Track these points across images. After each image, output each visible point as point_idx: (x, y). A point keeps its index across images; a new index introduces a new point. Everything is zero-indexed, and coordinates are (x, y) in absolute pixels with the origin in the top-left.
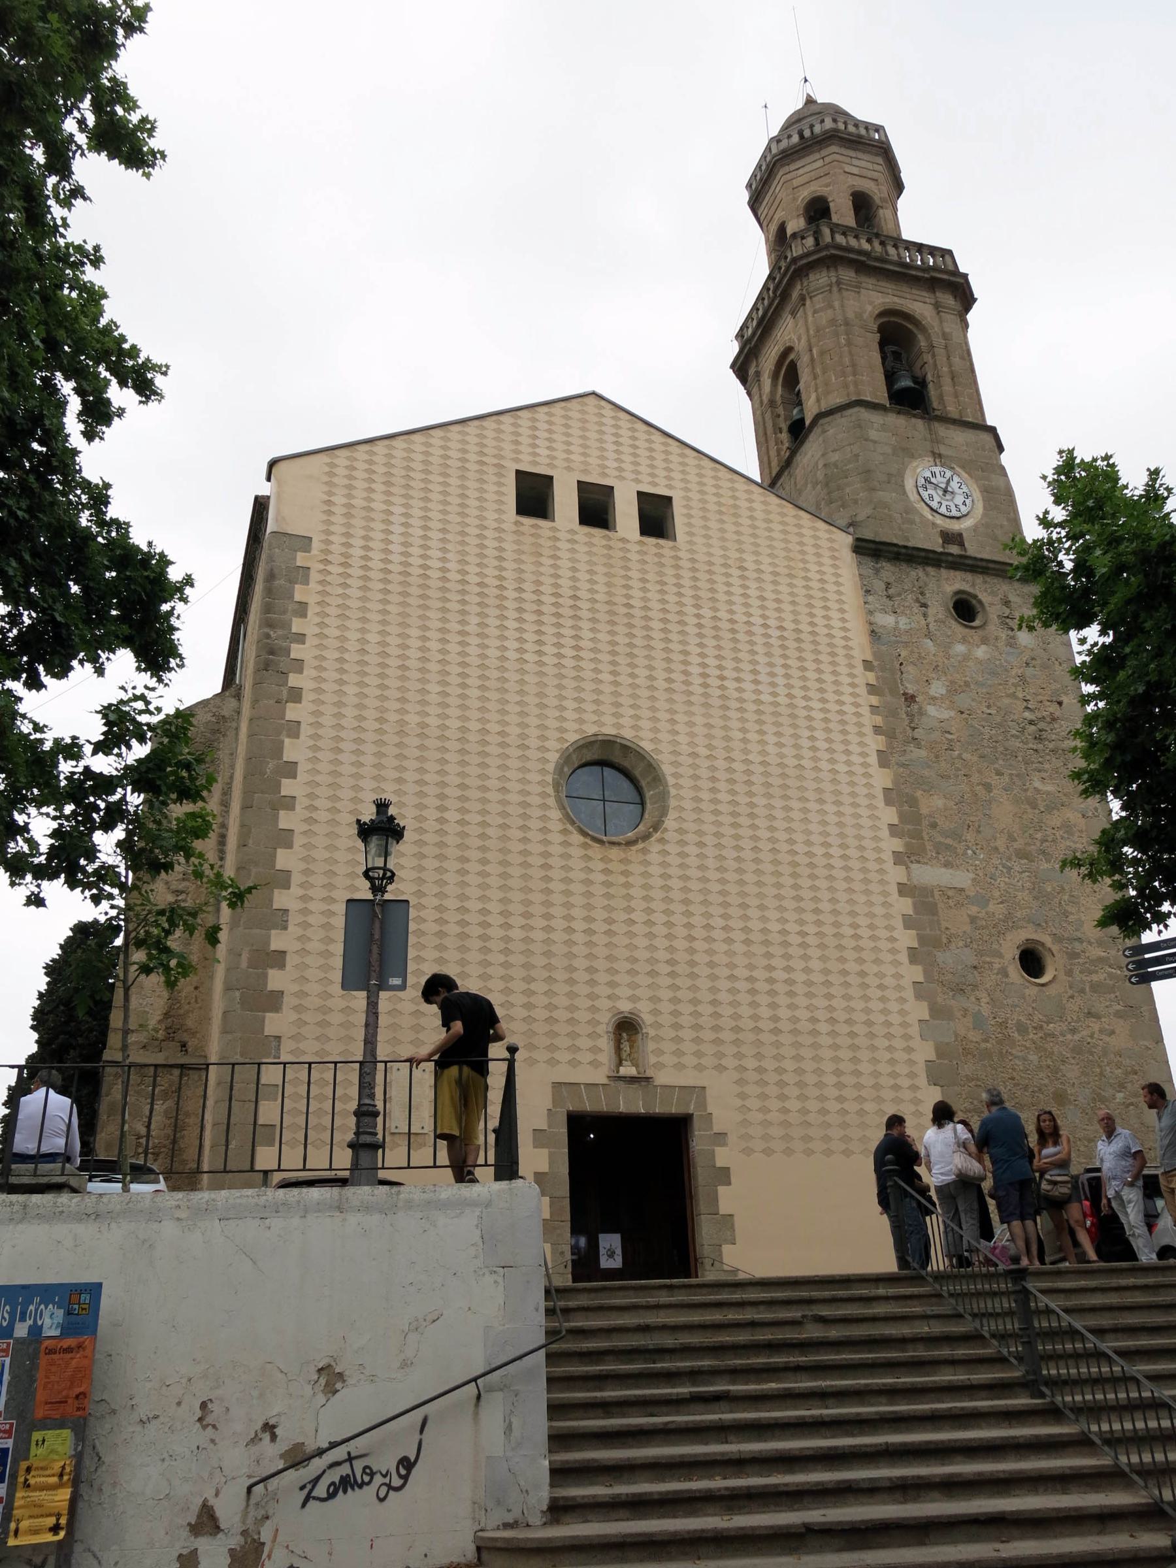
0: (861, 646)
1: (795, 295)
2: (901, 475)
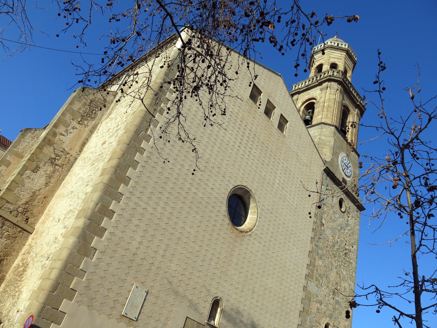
1: (325, 85)
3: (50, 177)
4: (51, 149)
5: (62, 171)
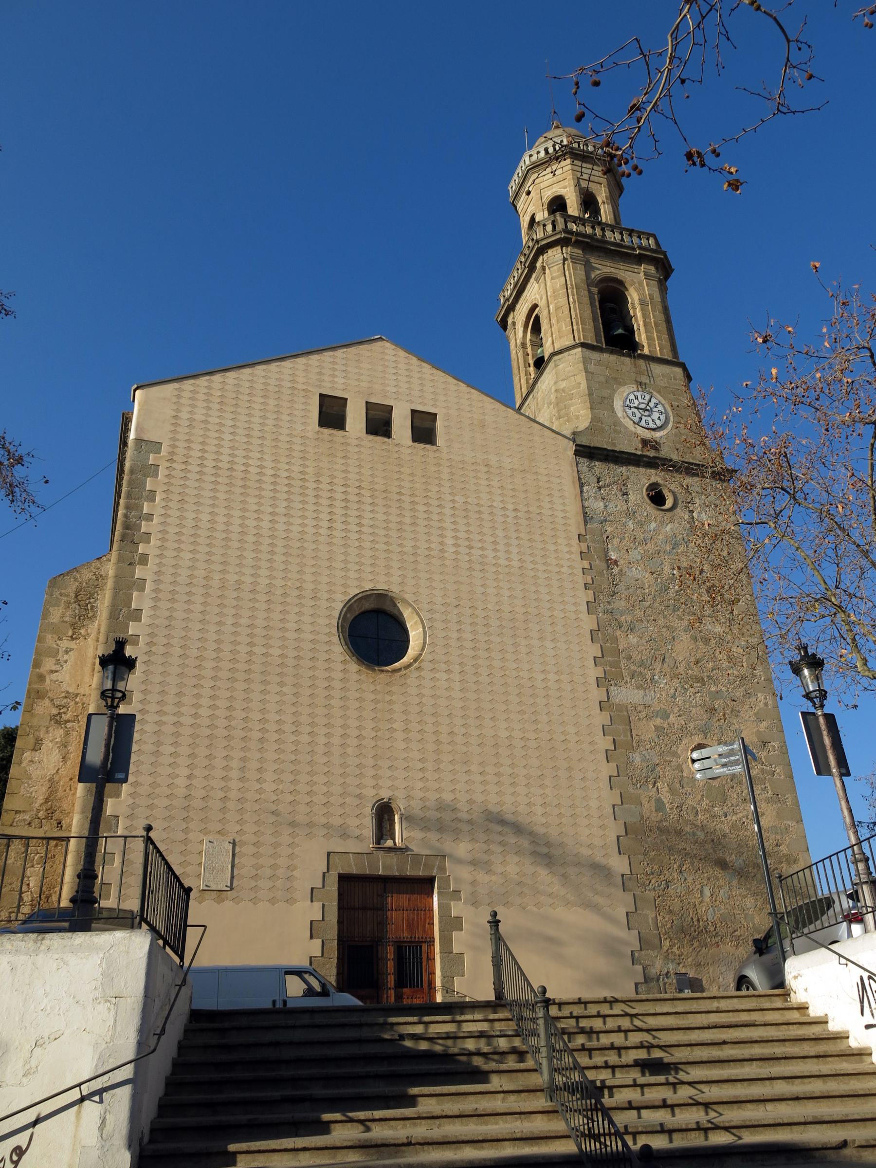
0: (575, 524)
1: (538, 265)
2: (611, 398)
3: (64, 745)
4: (47, 702)
5: (79, 727)
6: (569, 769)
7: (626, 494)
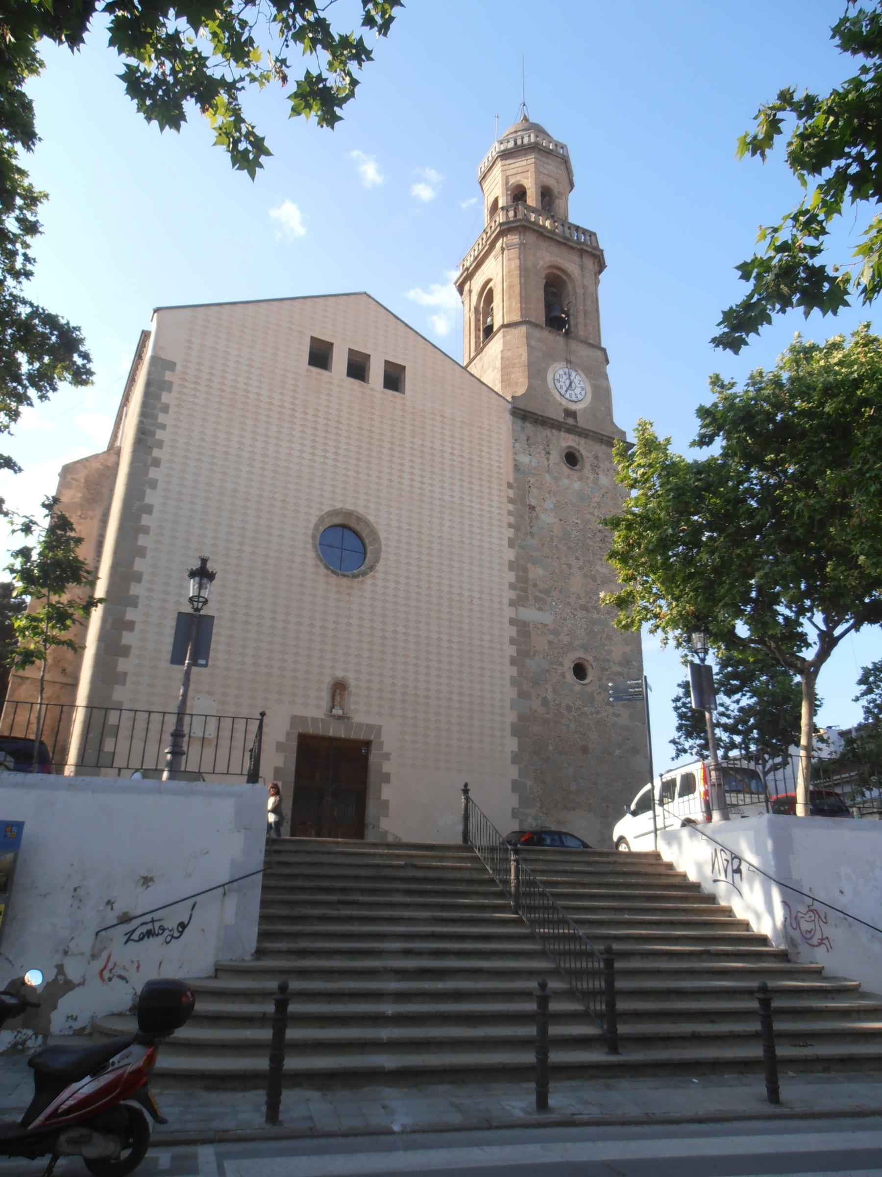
2: (545, 371)
6: (482, 668)
7: (548, 453)
